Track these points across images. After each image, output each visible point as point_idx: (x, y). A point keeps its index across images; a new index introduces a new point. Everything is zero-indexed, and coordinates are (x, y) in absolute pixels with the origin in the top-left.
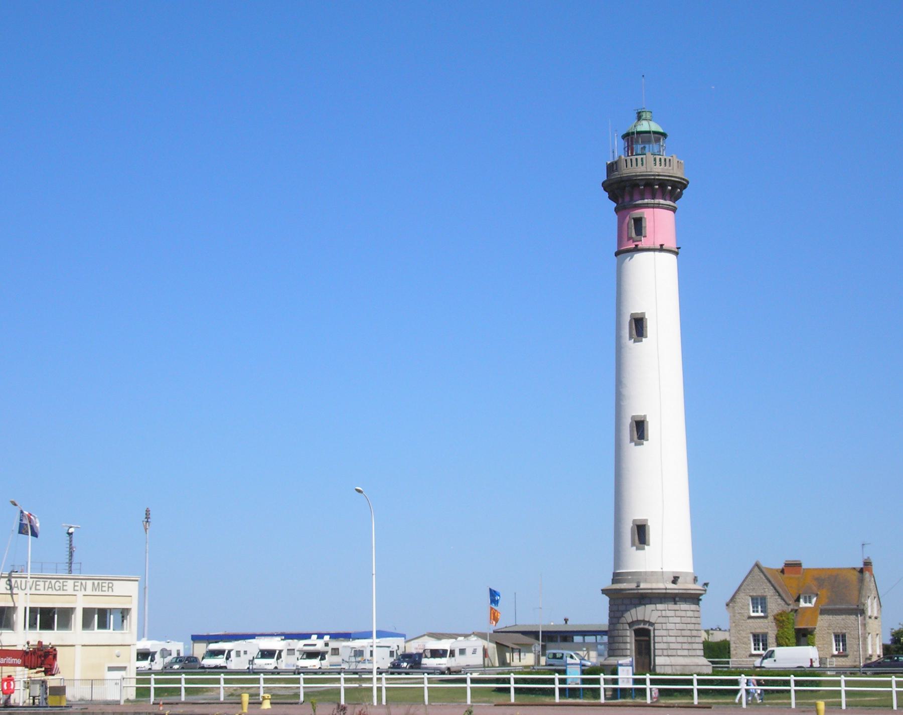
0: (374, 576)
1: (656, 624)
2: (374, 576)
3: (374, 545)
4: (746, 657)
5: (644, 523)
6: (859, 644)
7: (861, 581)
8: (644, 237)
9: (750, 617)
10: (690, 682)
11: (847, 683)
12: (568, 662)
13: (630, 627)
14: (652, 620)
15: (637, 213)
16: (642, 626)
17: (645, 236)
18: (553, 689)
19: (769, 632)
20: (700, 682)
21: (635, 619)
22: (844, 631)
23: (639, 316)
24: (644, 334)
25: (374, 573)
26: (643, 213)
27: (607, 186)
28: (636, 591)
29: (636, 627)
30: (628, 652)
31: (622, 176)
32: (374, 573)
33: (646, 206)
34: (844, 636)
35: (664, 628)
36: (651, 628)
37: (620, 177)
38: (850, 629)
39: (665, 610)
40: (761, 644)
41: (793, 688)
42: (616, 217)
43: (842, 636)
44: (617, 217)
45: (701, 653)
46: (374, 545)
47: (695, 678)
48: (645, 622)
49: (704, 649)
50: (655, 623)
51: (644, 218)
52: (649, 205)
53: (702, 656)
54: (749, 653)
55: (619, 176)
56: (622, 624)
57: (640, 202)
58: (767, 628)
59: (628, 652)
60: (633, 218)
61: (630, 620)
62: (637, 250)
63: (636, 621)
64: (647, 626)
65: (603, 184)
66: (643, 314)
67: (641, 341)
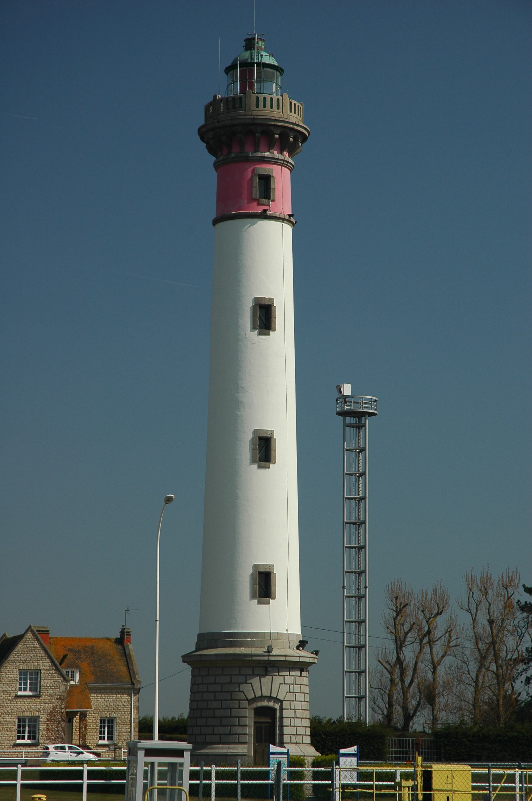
0: (158, 622)
1: (284, 702)
2: (158, 622)
3: (158, 580)
4: (9, 747)
5: (270, 571)
6: (130, 732)
7: (127, 657)
8: (272, 201)
9: (17, 697)
10: (79, 775)
11: (220, 775)
12: (271, 751)
13: (249, 704)
14: (281, 697)
15: (264, 169)
16: (265, 703)
17: (274, 201)
18: (81, 785)
19: (41, 716)
20: (92, 775)
21: (258, 694)
22: (113, 715)
23: (267, 303)
24: (273, 326)
25: (158, 619)
26: (272, 171)
27: (203, 133)
28: (266, 658)
29: (259, 704)
30: (246, 739)
31: (255, 117)
32: (158, 619)
33: (275, 162)
34: (111, 721)
35: (292, 707)
36: (277, 706)
37: (254, 118)
38: (121, 713)
39: (293, 684)
40: (106, 728)
41: (85, 782)
42: (214, 175)
43: (108, 721)
44: (217, 174)
45: (308, 740)
46: (158, 580)
47: (20, 768)
48: (270, 698)
49: (312, 736)
50: (284, 700)
51: (273, 177)
52: (279, 161)
53: (310, 744)
54: (12, 743)
55: (252, 117)
56: (239, 700)
57: (266, 154)
58: (39, 711)
59: (246, 739)
60: (259, 174)
61: (251, 696)
62: (264, 216)
63: (273, 698)
64: (271, 704)
65: (199, 130)
66: (272, 300)
67: (269, 335)
